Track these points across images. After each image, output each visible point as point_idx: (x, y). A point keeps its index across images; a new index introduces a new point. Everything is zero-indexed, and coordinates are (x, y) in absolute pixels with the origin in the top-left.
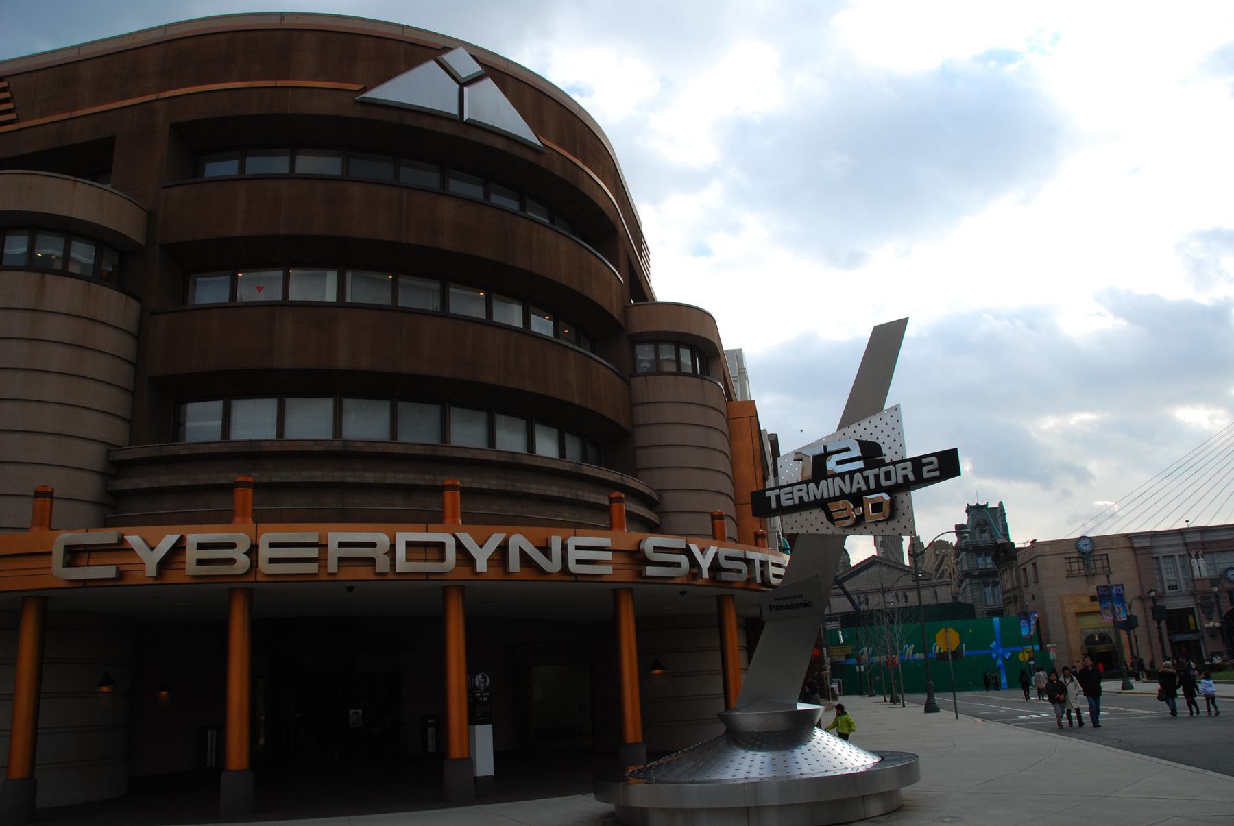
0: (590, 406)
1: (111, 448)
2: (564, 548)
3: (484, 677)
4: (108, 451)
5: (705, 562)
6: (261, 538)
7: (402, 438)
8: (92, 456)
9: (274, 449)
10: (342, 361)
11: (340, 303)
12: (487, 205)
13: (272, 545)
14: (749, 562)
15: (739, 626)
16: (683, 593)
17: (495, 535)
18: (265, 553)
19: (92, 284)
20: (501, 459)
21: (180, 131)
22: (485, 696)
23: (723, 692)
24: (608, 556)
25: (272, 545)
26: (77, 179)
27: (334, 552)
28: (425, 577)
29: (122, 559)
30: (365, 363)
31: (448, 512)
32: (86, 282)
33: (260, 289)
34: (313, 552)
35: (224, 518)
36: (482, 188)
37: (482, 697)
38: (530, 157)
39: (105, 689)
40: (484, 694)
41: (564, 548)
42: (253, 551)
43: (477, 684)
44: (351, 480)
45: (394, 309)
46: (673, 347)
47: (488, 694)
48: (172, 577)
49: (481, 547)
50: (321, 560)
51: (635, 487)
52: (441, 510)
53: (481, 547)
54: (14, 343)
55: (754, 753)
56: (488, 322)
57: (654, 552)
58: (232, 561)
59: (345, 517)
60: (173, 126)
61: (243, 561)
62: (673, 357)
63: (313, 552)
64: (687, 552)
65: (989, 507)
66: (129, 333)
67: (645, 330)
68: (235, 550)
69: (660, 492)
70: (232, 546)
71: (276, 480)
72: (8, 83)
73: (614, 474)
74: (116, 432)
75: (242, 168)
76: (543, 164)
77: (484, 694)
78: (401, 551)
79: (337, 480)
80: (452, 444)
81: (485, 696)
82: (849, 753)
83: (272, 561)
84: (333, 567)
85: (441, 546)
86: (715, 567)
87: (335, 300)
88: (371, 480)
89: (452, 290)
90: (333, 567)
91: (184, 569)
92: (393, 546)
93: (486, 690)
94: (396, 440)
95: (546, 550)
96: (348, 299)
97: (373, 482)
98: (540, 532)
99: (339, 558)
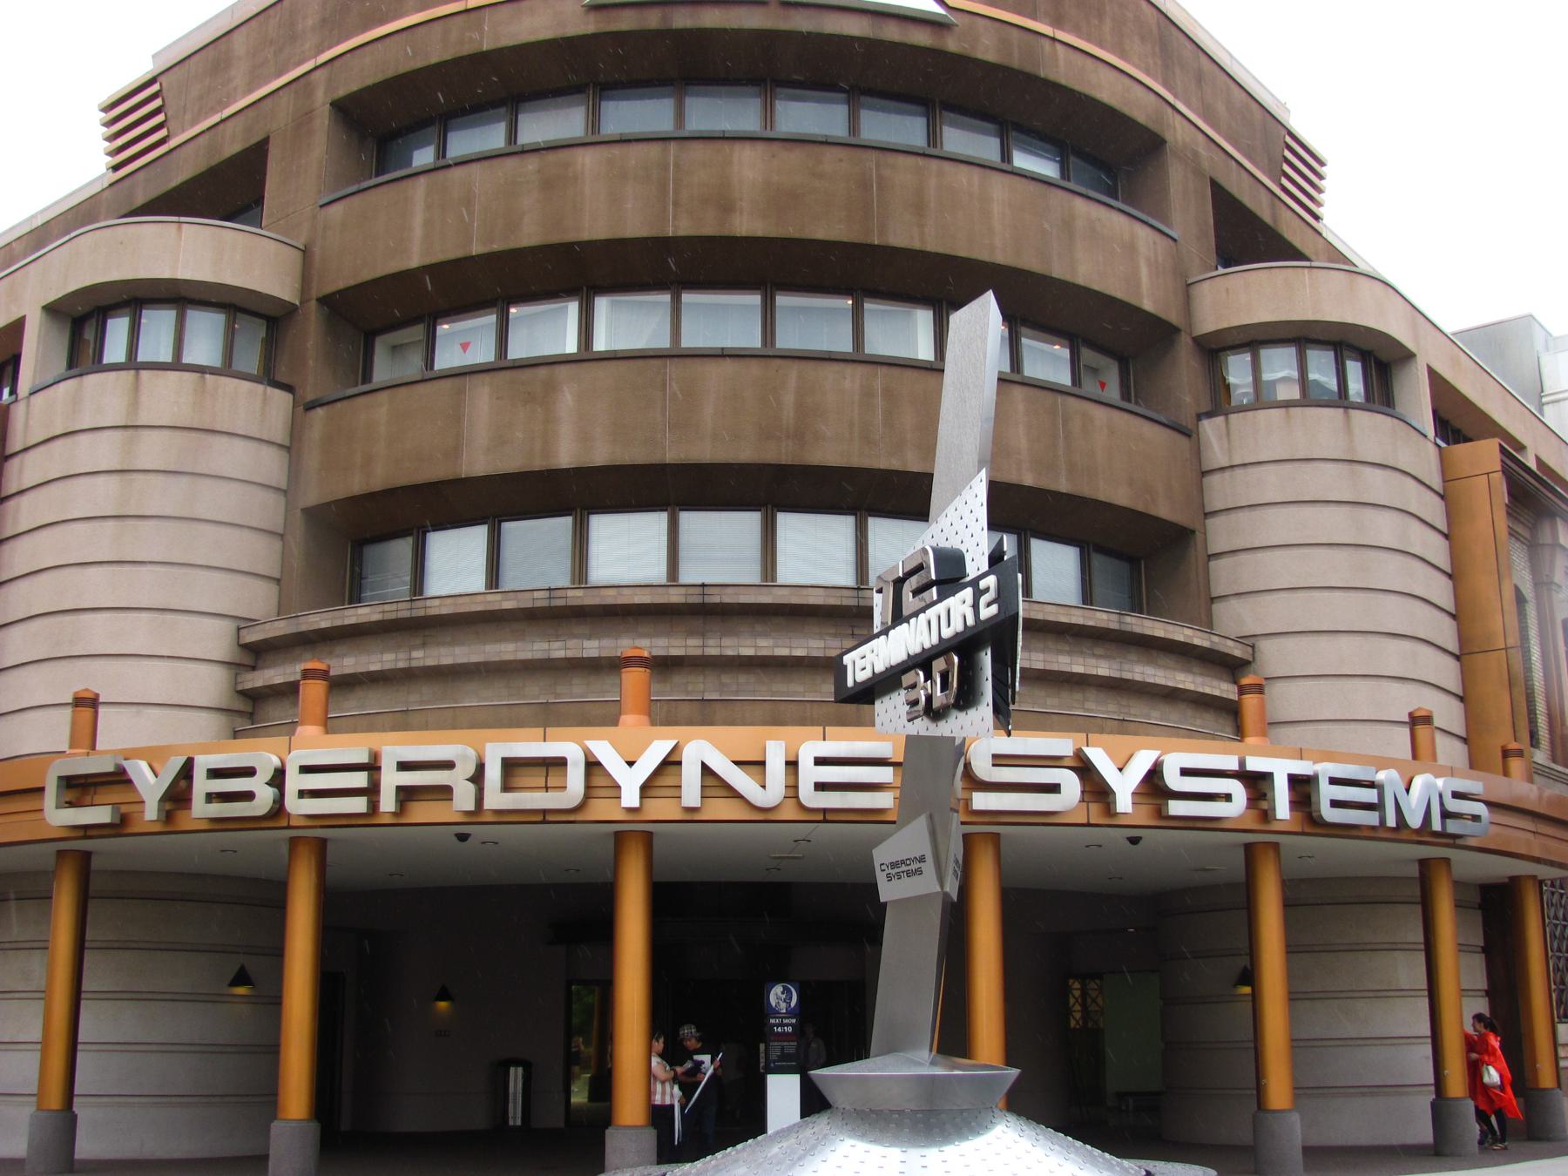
0: (1063, 486)
1: (244, 623)
2: (792, 765)
3: (786, 990)
4: (239, 629)
5: (1124, 786)
6: (685, 749)
7: (513, 577)
8: (216, 640)
9: (444, 611)
10: (566, 456)
11: (586, 356)
12: (449, 166)
13: (820, 761)
14: (1257, 784)
15: (1459, 905)
16: (1134, 841)
17: (656, 742)
18: (810, 774)
19: (207, 376)
20: (832, 601)
21: (347, 110)
22: (787, 1025)
23: (1428, 1033)
24: (884, 774)
25: (820, 761)
26: (183, 219)
27: (391, 779)
28: (540, 818)
29: (117, 795)
30: (601, 456)
31: (628, 702)
32: (199, 375)
33: (465, 346)
34: (359, 780)
35: (607, 717)
36: (846, 107)
37: (782, 1025)
38: (921, 37)
39: (241, 990)
40: (786, 1021)
41: (792, 765)
42: (278, 778)
43: (773, 1004)
44: (560, 654)
45: (677, 354)
46: (1331, 354)
47: (794, 1021)
48: (186, 821)
49: (631, 764)
50: (372, 791)
51: (1181, 639)
52: (618, 699)
53: (631, 764)
54: (101, 479)
55: (1062, 1161)
56: (858, 358)
57: (994, 765)
58: (248, 796)
59: (403, 722)
60: (334, 104)
61: (464, 798)
62: (1295, 374)
63: (359, 780)
64: (1084, 769)
65: (332, 673)
66: (273, 443)
67: (1225, 325)
68: (255, 777)
69: (1249, 641)
70: (249, 772)
71: (447, 660)
72: (161, 85)
73: (1098, 614)
74: (256, 600)
75: (442, 152)
76: (952, 44)
77: (786, 1021)
78: (493, 774)
79: (539, 655)
80: (780, 581)
81: (787, 1025)
82: (902, 1167)
83: (302, 794)
84: (388, 803)
85: (561, 763)
86: (1153, 784)
87: (575, 351)
88: (594, 653)
89: (867, 306)
90: (388, 803)
91: (42, 810)
92: (481, 768)
93: (790, 1013)
94: (776, 581)
95: (756, 766)
96: (600, 344)
97: (597, 655)
98: (743, 737)
99: (397, 787)
